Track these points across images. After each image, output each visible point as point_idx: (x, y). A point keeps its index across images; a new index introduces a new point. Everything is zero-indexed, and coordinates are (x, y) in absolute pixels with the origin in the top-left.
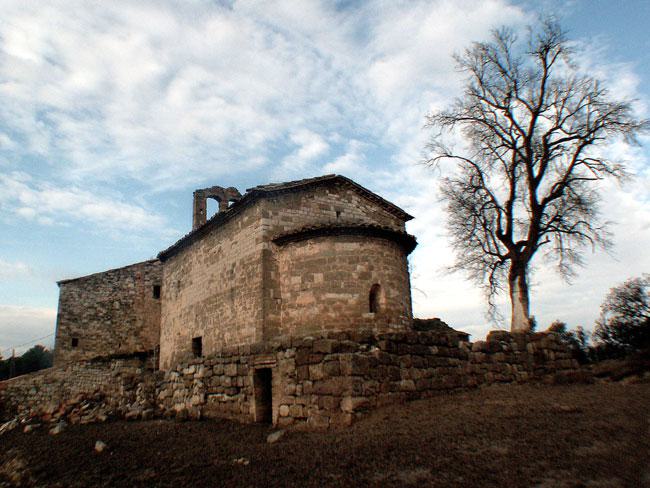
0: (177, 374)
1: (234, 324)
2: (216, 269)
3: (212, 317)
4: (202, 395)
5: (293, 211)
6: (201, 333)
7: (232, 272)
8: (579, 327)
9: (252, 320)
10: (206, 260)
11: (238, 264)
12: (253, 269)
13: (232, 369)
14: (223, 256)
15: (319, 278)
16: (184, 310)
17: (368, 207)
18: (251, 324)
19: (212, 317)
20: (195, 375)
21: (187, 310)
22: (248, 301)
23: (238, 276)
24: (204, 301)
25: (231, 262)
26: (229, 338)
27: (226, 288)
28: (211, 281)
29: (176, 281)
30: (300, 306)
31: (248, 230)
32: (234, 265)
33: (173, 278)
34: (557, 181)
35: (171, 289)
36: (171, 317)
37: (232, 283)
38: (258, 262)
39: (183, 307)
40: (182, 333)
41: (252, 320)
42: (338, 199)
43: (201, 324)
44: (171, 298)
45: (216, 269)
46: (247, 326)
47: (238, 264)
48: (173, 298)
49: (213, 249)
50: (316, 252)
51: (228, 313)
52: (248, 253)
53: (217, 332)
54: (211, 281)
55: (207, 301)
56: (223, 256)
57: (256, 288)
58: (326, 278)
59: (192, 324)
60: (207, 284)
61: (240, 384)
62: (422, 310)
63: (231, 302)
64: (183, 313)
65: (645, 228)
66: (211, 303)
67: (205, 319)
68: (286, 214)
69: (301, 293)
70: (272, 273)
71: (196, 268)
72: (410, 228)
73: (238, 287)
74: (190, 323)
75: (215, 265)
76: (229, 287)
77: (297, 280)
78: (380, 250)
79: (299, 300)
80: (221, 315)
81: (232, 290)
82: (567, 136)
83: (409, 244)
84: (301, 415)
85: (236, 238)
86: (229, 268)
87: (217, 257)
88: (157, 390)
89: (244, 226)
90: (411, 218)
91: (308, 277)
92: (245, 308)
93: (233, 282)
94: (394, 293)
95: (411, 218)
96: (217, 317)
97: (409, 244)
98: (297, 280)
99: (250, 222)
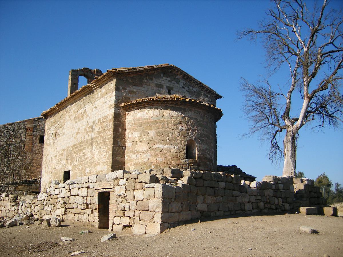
0: (47, 195)
1: (92, 163)
2: (82, 125)
3: (77, 157)
4: (63, 209)
5: (137, 88)
6: (69, 168)
7: (92, 127)
8: (331, 180)
9: (104, 160)
10: (75, 118)
11: (97, 122)
12: (107, 125)
13: (84, 192)
14: (87, 116)
15: (152, 133)
16: (59, 152)
17: (191, 88)
18: (103, 163)
19: (77, 157)
20: (59, 196)
21: (61, 152)
22: (102, 147)
23: (96, 130)
24: (72, 147)
25: (92, 120)
26: (89, 172)
27: (87, 138)
28: (78, 133)
29: (54, 132)
30: (138, 152)
31: (102, 100)
32: (94, 122)
33: (52, 130)
34: (323, 79)
35: (50, 138)
36: (50, 157)
37: (93, 135)
38: (110, 121)
39: (58, 150)
40: (57, 168)
41: (104, 160)
42: (169, 81)
43: (70, 162)
44: (50, 144)
45: (82, 125)
46: (101, 164)
47: (97, 122)
48: (52, 143)
49: (80, 111)
50: (152, 115)
51: (89, 155)
52: (103, 115)
53: (81, 167)
54: (78, 133)
55: (75, 146)
56: (87, 116)
57: (108, 139)
58: (157, 134)
59: (64, 162)
60: (75, 135)
61: (89, 202)
62: (222, 161)
63: (91, 147)
64: (58, 154)
65: (161, 195)
66: (78, 147)
67: (72, 159)
68: (132, 89)
69: (140, 143)
70: (120, 130)
71: (68, 124)
72: (220, 105)
73: (96, 137)
74: (63, 161)
75: (81, 122)
76: (90, 138)
77: (137, 134)
78: (196, 117)
79: (137, 148)
80: (84, 155)
81: (92, 139)
82: (337, 49)
83: (218, 115)
84: (128, 224)
85: (97, 104)
86: (91, 124)
87: (83, 116)
88: (33, 205)
89: (102, 96)
90: (220, 97)
91: (144, 132)
92: (100, 152)
93: (93, 134)
94: (204, 147)
95: (220, 97)
96: (81, 158)
97: (218, 115)
98: (137, 134)
99: (106, 93)
